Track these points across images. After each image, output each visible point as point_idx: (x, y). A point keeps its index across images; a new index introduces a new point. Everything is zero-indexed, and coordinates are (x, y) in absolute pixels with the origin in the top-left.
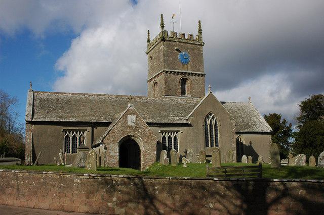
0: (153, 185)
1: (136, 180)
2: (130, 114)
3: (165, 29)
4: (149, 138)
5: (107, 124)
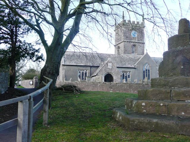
2: (109, 63)
3: (125, 19)
4: (117, 74)
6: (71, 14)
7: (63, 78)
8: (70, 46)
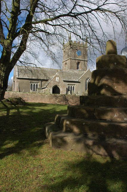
0: (68, 97)
1: (64, 96)
2: (57, 77)
4: (64, 86)
5: (47, 80)
6: (17, 33)
7: (17, 89)
8: (18, 62)
